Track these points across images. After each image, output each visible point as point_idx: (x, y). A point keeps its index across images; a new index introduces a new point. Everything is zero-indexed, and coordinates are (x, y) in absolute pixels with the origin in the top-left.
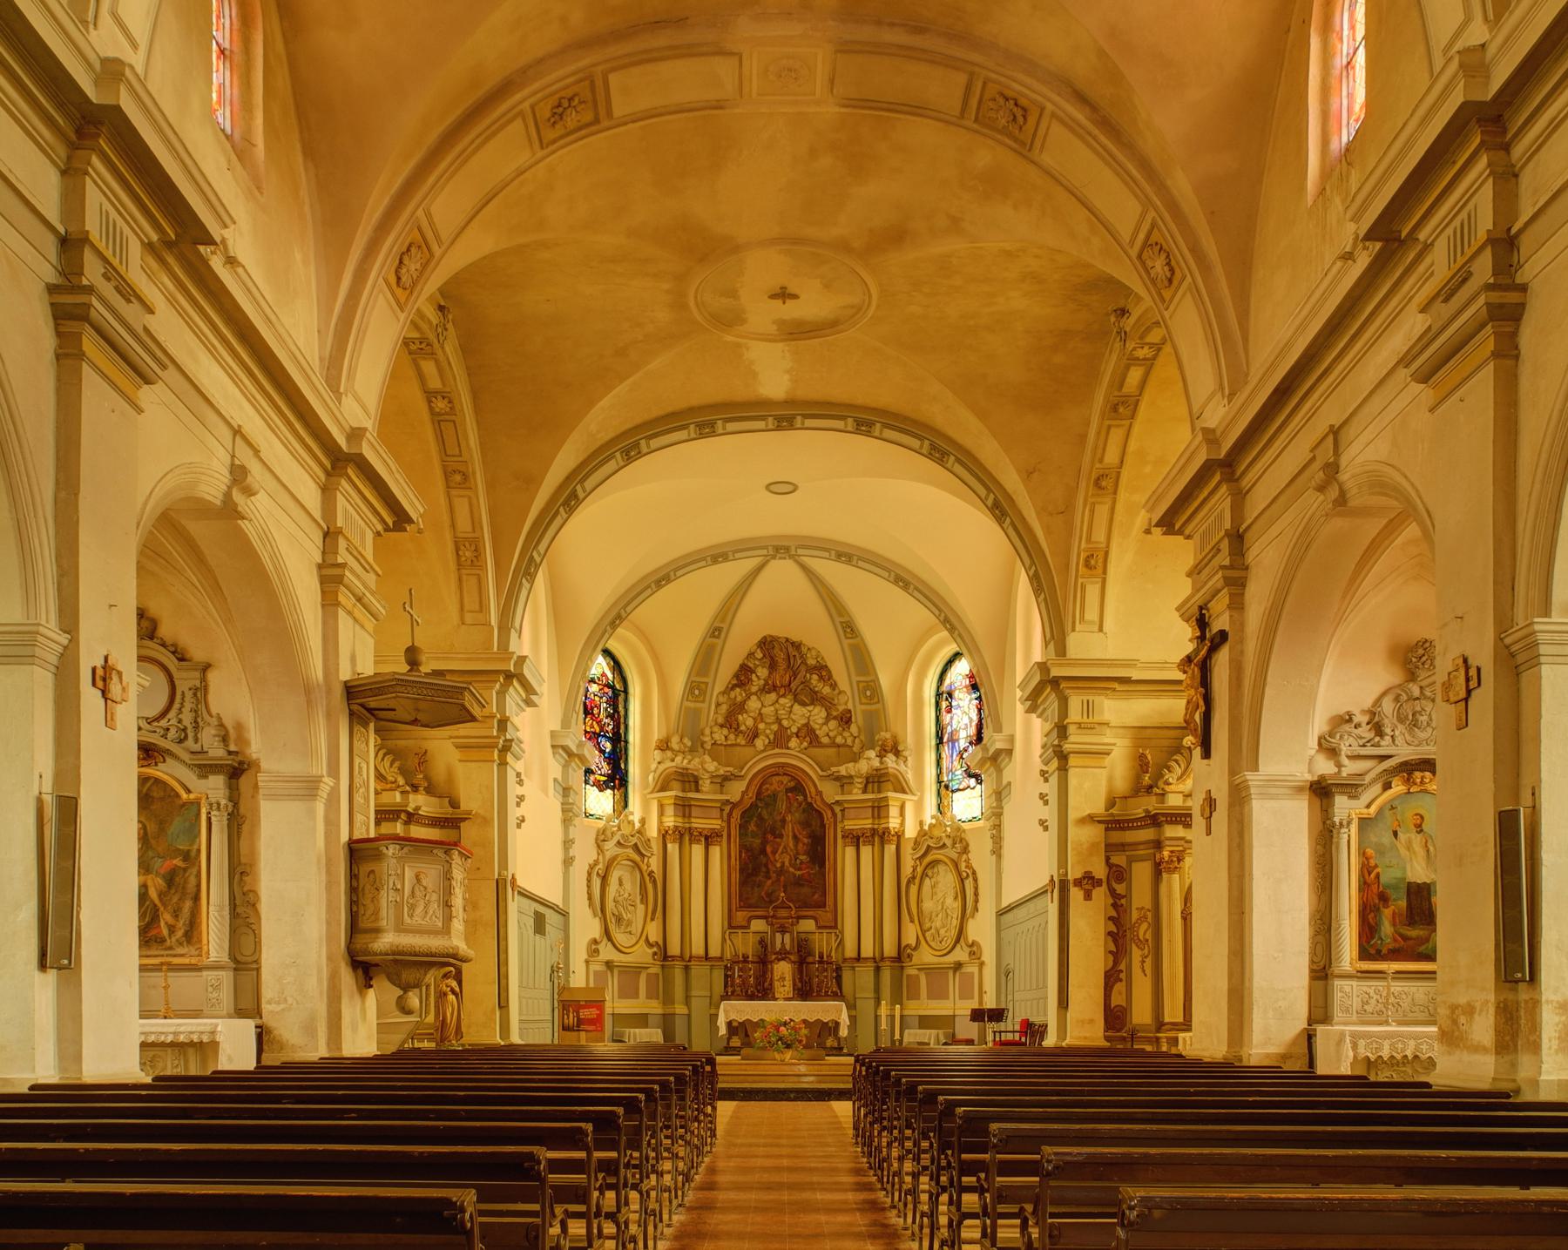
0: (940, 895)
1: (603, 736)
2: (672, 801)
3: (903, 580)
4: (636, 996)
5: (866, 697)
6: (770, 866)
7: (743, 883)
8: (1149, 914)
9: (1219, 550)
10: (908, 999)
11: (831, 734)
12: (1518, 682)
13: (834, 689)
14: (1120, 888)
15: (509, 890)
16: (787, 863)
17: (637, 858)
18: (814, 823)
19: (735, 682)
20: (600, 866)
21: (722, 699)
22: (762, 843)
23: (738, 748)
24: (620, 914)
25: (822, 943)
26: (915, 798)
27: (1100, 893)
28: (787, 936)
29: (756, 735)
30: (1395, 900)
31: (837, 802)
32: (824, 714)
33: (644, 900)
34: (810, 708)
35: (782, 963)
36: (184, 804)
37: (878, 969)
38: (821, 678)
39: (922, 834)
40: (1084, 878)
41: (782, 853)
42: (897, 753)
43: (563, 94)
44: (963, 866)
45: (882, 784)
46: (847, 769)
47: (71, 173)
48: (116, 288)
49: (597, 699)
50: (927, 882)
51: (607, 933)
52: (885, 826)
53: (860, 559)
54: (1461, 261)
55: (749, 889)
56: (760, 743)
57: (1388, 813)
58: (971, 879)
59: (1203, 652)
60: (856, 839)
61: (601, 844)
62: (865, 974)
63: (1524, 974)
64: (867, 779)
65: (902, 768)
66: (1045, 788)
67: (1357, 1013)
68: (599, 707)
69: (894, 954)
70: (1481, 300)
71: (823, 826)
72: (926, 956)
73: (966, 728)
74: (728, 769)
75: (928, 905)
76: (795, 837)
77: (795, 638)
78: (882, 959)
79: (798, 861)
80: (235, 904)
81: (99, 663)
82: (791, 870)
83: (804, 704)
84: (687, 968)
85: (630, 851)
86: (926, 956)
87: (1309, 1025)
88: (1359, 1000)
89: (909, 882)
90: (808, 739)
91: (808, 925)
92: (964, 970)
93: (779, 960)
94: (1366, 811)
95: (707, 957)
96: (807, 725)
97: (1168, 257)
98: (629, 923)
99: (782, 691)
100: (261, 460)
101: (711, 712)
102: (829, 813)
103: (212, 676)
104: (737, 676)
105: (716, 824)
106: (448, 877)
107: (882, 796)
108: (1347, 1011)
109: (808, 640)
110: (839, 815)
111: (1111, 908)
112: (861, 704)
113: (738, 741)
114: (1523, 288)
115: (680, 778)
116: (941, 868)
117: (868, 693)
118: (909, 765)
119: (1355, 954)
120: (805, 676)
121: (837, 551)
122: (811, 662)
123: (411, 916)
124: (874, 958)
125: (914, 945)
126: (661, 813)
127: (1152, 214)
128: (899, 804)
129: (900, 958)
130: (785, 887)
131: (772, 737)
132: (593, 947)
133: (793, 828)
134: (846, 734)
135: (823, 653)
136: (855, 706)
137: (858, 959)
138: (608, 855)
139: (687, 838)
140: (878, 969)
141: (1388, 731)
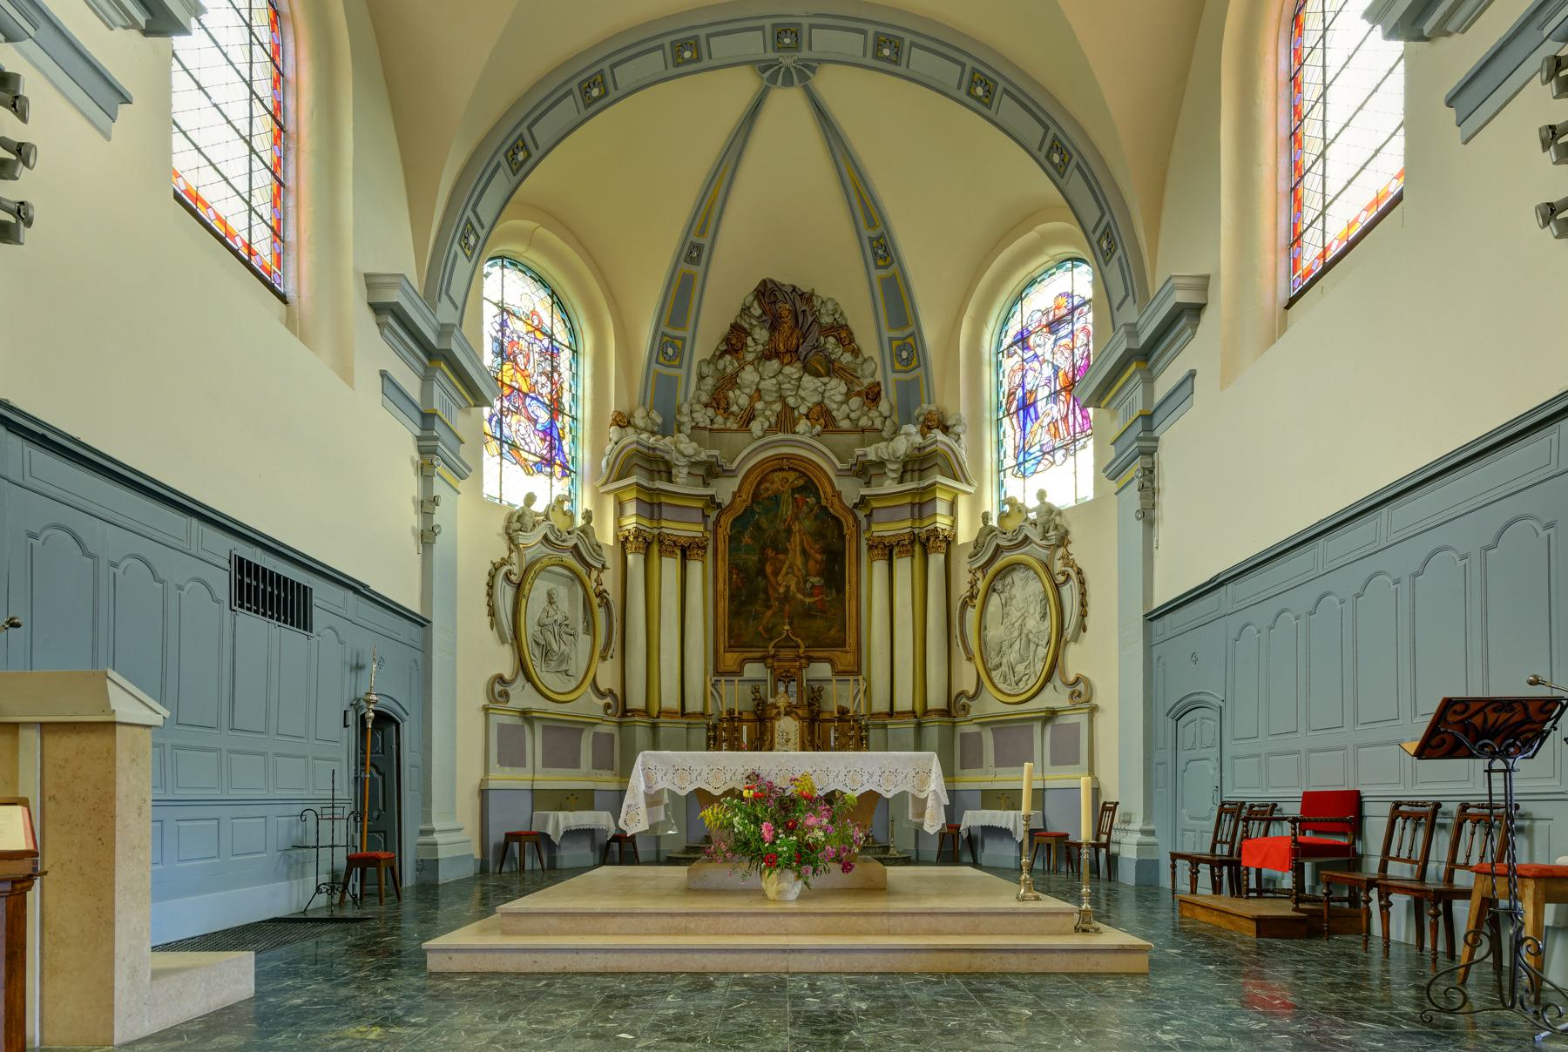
0: (1015, 614)
1: (533, 398)
2: (634, 495)
4: (575, 763)
6: (771, 592)
7: (734, 614)
10: (962, 767)
11: (853, 415)
13: (857, 357)
16: (793, 588)
18: (829, 534)
19: (724, 347)
21: (706, 370)
22: (760, 560)
23: (728, 435)
24: (548, 643)
25: (839, 695)
29: (752, 417)
32: (843, 388)
33: (590, 628)
34: (826, 380)
37: (919, 727)
38: (839, 340)
39: (987, 532)
41: (787, 573)
42: (946, 430)
44: (1058, 566)
45: (924, 473)
46: (877, 449)
47: (427, 379)
50: (995, 600)
51: (523, 667)
52: (932, 527)
55: (742, 622)
56: (756, 427)
60: (888, 551)
64: (905, 464)
65: (954, 445)
68: (527, 356)
69: (942, 705)
71: (842, 537)
72: (992, 705)
75: (994, 633)
76: (804, 552)
77: (805, 288)
78: (926, 712)
79: (808, 585)
82: (800, 596)
83: (817, 375)
84: (654, 727)
89: (965, 605)
90: (822, 421)
91: (822, 670)
92: (1060, 721)
95: (683, 713)
96: (820, 404)
98: (564, 658)
99: (787, 358)
101: (691, 389)
102: (851, 520)
104: (727, 340)
105: (689, 530)
109: (822, 292)
112: (894, 371)
113: (728, 425)
115: (646, 465)
116: (1018, 576)
117: (904, 354)
118: (963, 446)
122: (826, 320)
124: (913, 712)
125: (971, 691)
128: (948, 497)
129: (953, 709)
130: (791, 618)
131: (773, 420)
132: (498, 688)
133: (802, 542)
134: (873, 414)
135: (843, 306)
137: (891, 713)
138: (529, 555)
139: (655, 548)
140: (919, 727)
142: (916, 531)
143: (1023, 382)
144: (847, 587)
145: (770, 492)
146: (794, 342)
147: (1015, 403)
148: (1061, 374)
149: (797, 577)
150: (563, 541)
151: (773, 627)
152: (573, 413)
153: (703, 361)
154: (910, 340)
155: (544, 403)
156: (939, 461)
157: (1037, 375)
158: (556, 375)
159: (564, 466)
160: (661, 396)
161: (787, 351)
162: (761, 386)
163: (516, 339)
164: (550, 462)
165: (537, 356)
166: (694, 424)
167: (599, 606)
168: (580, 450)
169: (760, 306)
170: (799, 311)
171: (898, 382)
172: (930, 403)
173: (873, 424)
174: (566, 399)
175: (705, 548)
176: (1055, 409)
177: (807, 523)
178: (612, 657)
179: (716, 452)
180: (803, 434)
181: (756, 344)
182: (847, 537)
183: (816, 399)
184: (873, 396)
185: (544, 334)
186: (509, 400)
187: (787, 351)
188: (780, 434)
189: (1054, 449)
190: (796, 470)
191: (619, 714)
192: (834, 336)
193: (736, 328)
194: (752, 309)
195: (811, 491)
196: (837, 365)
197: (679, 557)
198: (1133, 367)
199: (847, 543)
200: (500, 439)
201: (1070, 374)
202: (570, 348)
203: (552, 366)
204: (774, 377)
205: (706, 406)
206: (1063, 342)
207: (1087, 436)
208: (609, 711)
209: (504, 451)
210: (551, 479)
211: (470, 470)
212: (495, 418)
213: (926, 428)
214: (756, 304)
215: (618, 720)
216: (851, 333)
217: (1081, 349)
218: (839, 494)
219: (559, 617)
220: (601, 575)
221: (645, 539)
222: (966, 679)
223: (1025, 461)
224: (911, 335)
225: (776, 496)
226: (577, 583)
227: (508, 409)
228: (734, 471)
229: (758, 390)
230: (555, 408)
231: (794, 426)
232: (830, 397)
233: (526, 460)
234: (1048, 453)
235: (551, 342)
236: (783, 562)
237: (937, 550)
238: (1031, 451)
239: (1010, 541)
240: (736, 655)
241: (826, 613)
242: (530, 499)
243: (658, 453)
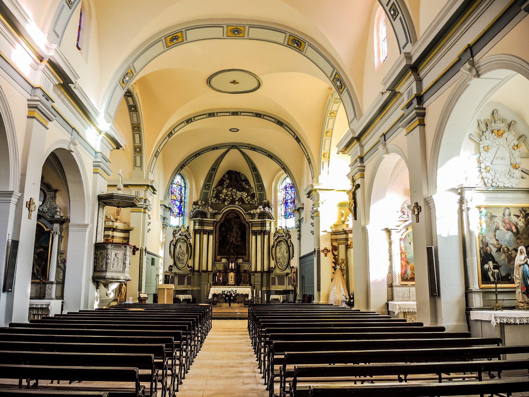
0: (282, 251)
3: (271, 156)
5: (260, 189)
6: (228, 242)
7: (219, 247)
8: (345, 261)
9: (357, 161)
12: (430, 211)
14: (336, 253)
15: (144, 252)
16: (234, 241)
17: (186, 239)
20: (174, 242)
21: (214, 189)
26: (275, 221)
27: (330, 254)
28: (233, 264)
30: (411, 263)
31: (250, 221)
32: (246, 194)
36: (46, 232)
38: (246, 183)
40: (325, 250)
42: (269, 207)
43: (173, 35)
44: (289, 242)
46: (253, 211)
48: (46, 98)
49: (175, 189)
53: (258, 149)
54: (410, 99)
56: (226, 203)
57: (408, 237)
58: (291, 247)
59: (353, 190)
60: (255, 233)
62: (258, 277)
63: (436, 294)
65: (270, 211)
66: (313, 221)
67: (402, 297)
68: (176, 192)
70: (414, 111)
72: (278, 271)
73: (290, 200)
74: (216, 211)
75: (278, 255)
76: (236, 232)
78: (264, 272)
80: (58, 263)
81: (28, 200)
82: (235, 243)
83: (240, 191)
85: (184, 237)
86: (278, 271)
87: (388, 301)
88: (402, 293)
91: (240, 261)
93: (231, 272)
94: (401, 237)
97: (340, 82)
98: (183, 260)
100: (79, 135)
101: (211, 193)
103: (57, 194)
105: (211, 228)
106: (125, 255)
107: (264, 220)
108: (398, 297)
109: (242, 172)
110: (251, 226)
111: (333, 259)
112: (258, 191)
114: (425, 109)
116: (282, 243)
117: (260, 188)
119: (400, 279)
120: (241, 183)
121: (251, 147)
123: (113, 267)
126: (195, 225)
127: (335, 71)
128: (269, 222)
131: (230, 201)
132: (170, 268)
135: (246, 176)
136: (256, 192)
138: (177, 238)
139: (202, 233)
140: (262, 276)
141: (406, 213)
159: (182, 214)
160: (204, 198)
168: (187, 210)
171: (259, 193)
184: (253, 196)
190: (235, 213)
198: (355, 141)
206: (292, 192)
222: (273, 264)
223: (286, 215)
229: (227, 194)
236: (232, 235)
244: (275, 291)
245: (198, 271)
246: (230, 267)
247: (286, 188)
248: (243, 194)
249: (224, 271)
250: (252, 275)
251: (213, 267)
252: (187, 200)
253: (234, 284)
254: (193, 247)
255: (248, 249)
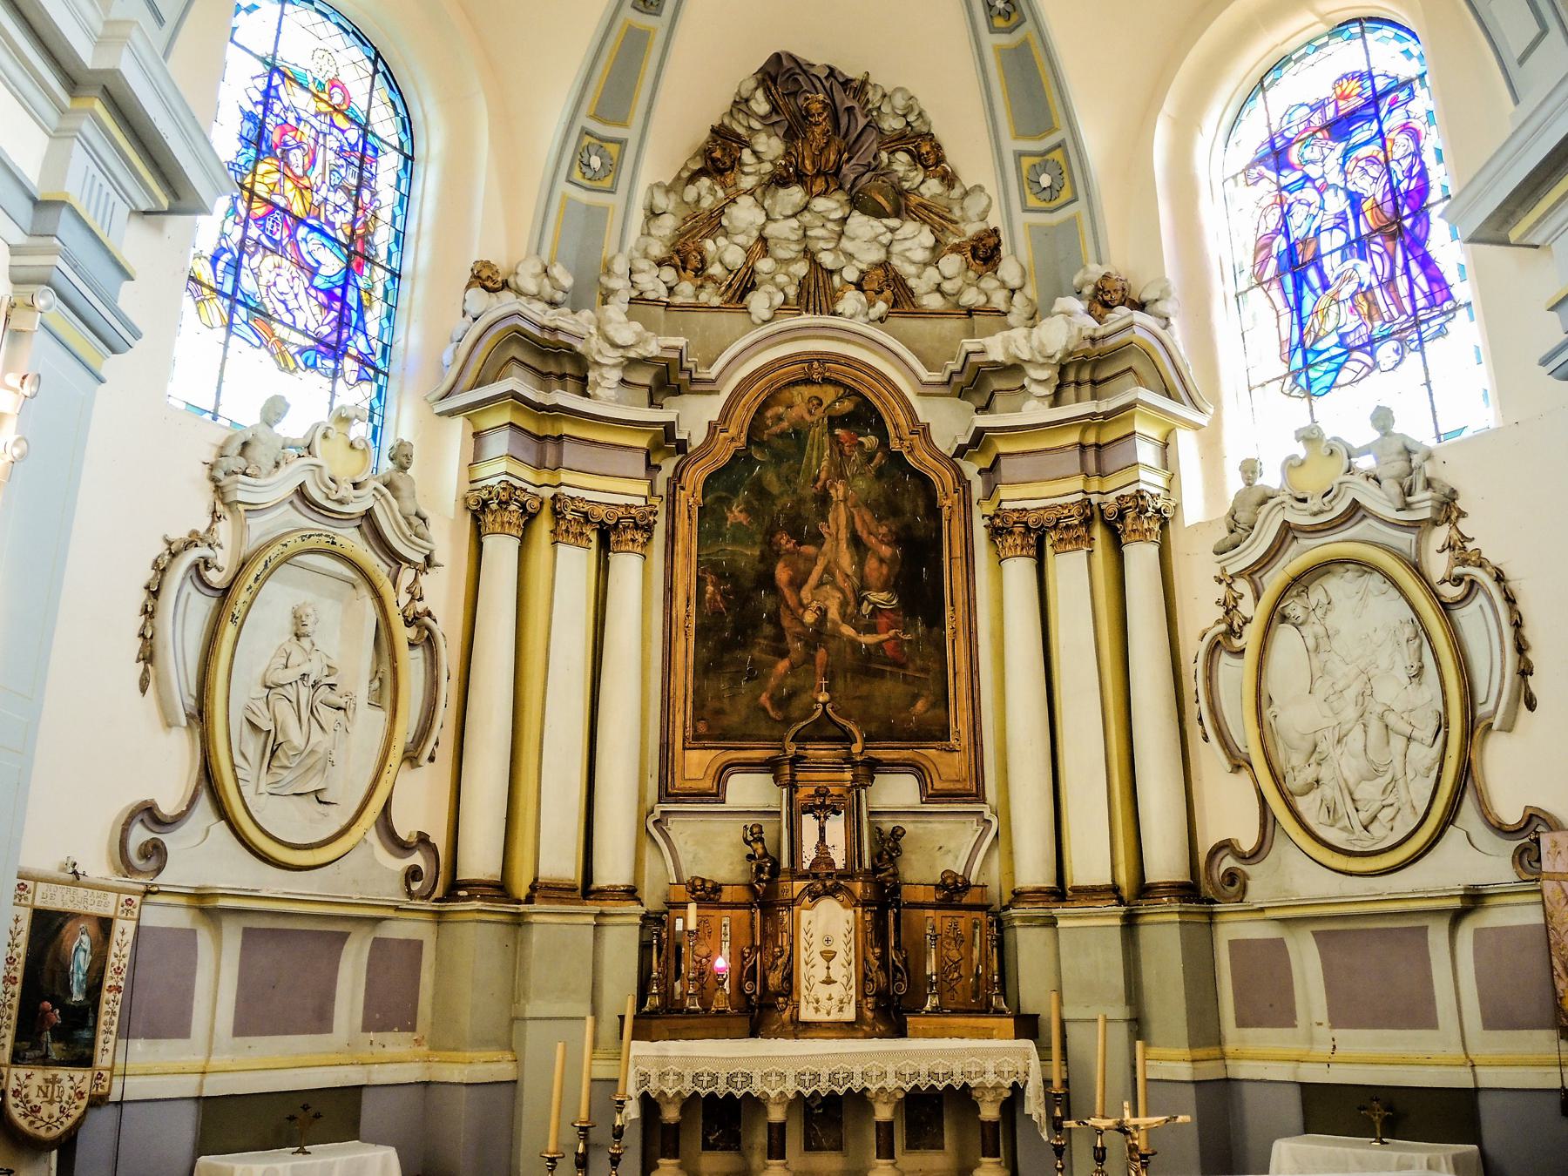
1: (313, 229)
7: (705, 669)
11: (947, 286)
13: (951, 186)
16: (833, 613)
18: (908, 506)
19: (696, 166)
22: (763, 558)
28: (836, 828)
32: (927, 238)
34: (893, 222)
35: (828, 907)
38: (917, 158)
41: (821, 584)
44: (1438, 565)
56: (759, 302)
61: (225, 481)
64: (1063, 369)
71: (934, 512)
76: (856, 542)
77: (853, 72)
78: (1144, 890)
79: (866, 609)
82: (848, 631)
83: (878, 213)
90: (888, 293)
93: (816, 896)
95: (587, 889)
96: (884, 265)
99: (819, 185)
102: (949, 478)
104: (706, 153)
109: (884, 78)
112: (1026, 210)
113: (703, 297)
116: (1338, 586)
122: (892, 124)
124: (1114, 889)
125: (1248, 843)
128: (1156, 433)
130: (830, 675)
131: (792, 291)
132: (140, 835)
133: (851, 520)
134: (989, 283)
135: (924, 102)
137: (1059, 892)
138: (259, 529)
139: (544, 525)
142: (1095, 499)
143: (1286, 225)
144: (948, 614)
145: (785, 424)
146: (832, 158)
147: (1273, 263)
148: (1366, 206)
149: (842, 591)
150: (340, 502)
151: (793, 694)
152: (394, 265)
153: (658, 185)
154: (1057, 155)
155: (335, 240)
156: (1134, 362)
157: (1313, 210)
158: (366, 194)
159: (364, 361)
161: (819, 173)
162: (768, 232)
163: (292, 121)
164: (335, 350)
165: (331, 156)
166: (634, 294)
167: (412, 645)
169: (767, 98)
170: (841, 109)
172: (1100, 263)
173: (988, 301)
174: (382, 237)
175: (648, 529)
176: (1364, 268)
177: (861, 484)
178: (431, 759)
179: (680, 342)
180: (852, 317)
181: (760, 160)
182: (945, 511)
183: (877, 255)
184: (985, 252)
185: (352, 121)
186: (263, 228)
187: (819, 173)
188: (805, 315)
189: (1371, 342)
190: (836, 383)
191: (439, 892)
192: (908, 151)
193: (721, 134)
194: (753, 104)
195: (870, 425)
196: (914, 200)
197: (594, 545)
199: (945, 524)
200: (232, 297)
201: (1388, 206)
202: (401, 151)
203: (360, 177)
204: (794, 215)
205: (660, 264)
206: (1364, 152)
207: (1443, 313)
208: (416, 886)
209: (236, 320)
210: (334, 382)
211: (137, 335)
212: (226, 257)
213: (1103, 298)
214: (760, 94)
215: (436, 907)
216: (939, 147)
217: (1406, 163)
218: (926, 429)
219: (316, 670)
220: (422, 578)
221: (523, 506)
223: (1307, 366)
224: (1059, 146)
225: (796, 432)
226: (365, 591)
227: (258, 243)
228: (713, 381)
229: (763, 239)
230: (357, 254)
231: (834, 304)
232: (902, 254)
233: (283, 342)
234: (1358, 348)
235: (365, 136)
237: (1143, 535)
238: (1320, 346)
239: (1315, 514)
240: (710, 755)
241: (903, 666)
242: (275, 410)
243: (561, 337)
244: (1304, 1086)
245: (500, 889)
246: (809, 853)
247: (1277, 156)
248: (899, 235)
249: (750, 887)
250: (1029, 921)
251: (649, 851)
252: (418, 258)
253: (850, 1014)
254: (449, 656)
255: (963, 684)
